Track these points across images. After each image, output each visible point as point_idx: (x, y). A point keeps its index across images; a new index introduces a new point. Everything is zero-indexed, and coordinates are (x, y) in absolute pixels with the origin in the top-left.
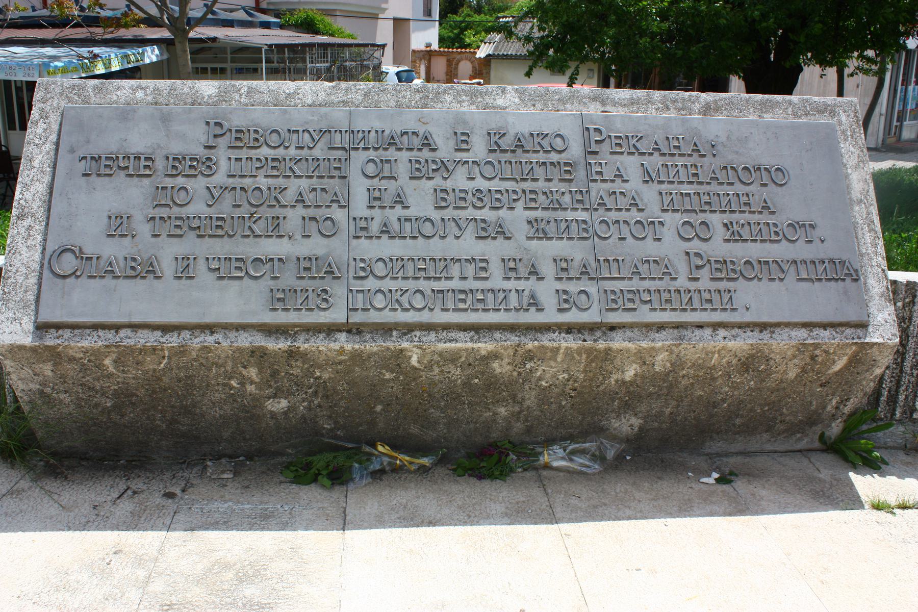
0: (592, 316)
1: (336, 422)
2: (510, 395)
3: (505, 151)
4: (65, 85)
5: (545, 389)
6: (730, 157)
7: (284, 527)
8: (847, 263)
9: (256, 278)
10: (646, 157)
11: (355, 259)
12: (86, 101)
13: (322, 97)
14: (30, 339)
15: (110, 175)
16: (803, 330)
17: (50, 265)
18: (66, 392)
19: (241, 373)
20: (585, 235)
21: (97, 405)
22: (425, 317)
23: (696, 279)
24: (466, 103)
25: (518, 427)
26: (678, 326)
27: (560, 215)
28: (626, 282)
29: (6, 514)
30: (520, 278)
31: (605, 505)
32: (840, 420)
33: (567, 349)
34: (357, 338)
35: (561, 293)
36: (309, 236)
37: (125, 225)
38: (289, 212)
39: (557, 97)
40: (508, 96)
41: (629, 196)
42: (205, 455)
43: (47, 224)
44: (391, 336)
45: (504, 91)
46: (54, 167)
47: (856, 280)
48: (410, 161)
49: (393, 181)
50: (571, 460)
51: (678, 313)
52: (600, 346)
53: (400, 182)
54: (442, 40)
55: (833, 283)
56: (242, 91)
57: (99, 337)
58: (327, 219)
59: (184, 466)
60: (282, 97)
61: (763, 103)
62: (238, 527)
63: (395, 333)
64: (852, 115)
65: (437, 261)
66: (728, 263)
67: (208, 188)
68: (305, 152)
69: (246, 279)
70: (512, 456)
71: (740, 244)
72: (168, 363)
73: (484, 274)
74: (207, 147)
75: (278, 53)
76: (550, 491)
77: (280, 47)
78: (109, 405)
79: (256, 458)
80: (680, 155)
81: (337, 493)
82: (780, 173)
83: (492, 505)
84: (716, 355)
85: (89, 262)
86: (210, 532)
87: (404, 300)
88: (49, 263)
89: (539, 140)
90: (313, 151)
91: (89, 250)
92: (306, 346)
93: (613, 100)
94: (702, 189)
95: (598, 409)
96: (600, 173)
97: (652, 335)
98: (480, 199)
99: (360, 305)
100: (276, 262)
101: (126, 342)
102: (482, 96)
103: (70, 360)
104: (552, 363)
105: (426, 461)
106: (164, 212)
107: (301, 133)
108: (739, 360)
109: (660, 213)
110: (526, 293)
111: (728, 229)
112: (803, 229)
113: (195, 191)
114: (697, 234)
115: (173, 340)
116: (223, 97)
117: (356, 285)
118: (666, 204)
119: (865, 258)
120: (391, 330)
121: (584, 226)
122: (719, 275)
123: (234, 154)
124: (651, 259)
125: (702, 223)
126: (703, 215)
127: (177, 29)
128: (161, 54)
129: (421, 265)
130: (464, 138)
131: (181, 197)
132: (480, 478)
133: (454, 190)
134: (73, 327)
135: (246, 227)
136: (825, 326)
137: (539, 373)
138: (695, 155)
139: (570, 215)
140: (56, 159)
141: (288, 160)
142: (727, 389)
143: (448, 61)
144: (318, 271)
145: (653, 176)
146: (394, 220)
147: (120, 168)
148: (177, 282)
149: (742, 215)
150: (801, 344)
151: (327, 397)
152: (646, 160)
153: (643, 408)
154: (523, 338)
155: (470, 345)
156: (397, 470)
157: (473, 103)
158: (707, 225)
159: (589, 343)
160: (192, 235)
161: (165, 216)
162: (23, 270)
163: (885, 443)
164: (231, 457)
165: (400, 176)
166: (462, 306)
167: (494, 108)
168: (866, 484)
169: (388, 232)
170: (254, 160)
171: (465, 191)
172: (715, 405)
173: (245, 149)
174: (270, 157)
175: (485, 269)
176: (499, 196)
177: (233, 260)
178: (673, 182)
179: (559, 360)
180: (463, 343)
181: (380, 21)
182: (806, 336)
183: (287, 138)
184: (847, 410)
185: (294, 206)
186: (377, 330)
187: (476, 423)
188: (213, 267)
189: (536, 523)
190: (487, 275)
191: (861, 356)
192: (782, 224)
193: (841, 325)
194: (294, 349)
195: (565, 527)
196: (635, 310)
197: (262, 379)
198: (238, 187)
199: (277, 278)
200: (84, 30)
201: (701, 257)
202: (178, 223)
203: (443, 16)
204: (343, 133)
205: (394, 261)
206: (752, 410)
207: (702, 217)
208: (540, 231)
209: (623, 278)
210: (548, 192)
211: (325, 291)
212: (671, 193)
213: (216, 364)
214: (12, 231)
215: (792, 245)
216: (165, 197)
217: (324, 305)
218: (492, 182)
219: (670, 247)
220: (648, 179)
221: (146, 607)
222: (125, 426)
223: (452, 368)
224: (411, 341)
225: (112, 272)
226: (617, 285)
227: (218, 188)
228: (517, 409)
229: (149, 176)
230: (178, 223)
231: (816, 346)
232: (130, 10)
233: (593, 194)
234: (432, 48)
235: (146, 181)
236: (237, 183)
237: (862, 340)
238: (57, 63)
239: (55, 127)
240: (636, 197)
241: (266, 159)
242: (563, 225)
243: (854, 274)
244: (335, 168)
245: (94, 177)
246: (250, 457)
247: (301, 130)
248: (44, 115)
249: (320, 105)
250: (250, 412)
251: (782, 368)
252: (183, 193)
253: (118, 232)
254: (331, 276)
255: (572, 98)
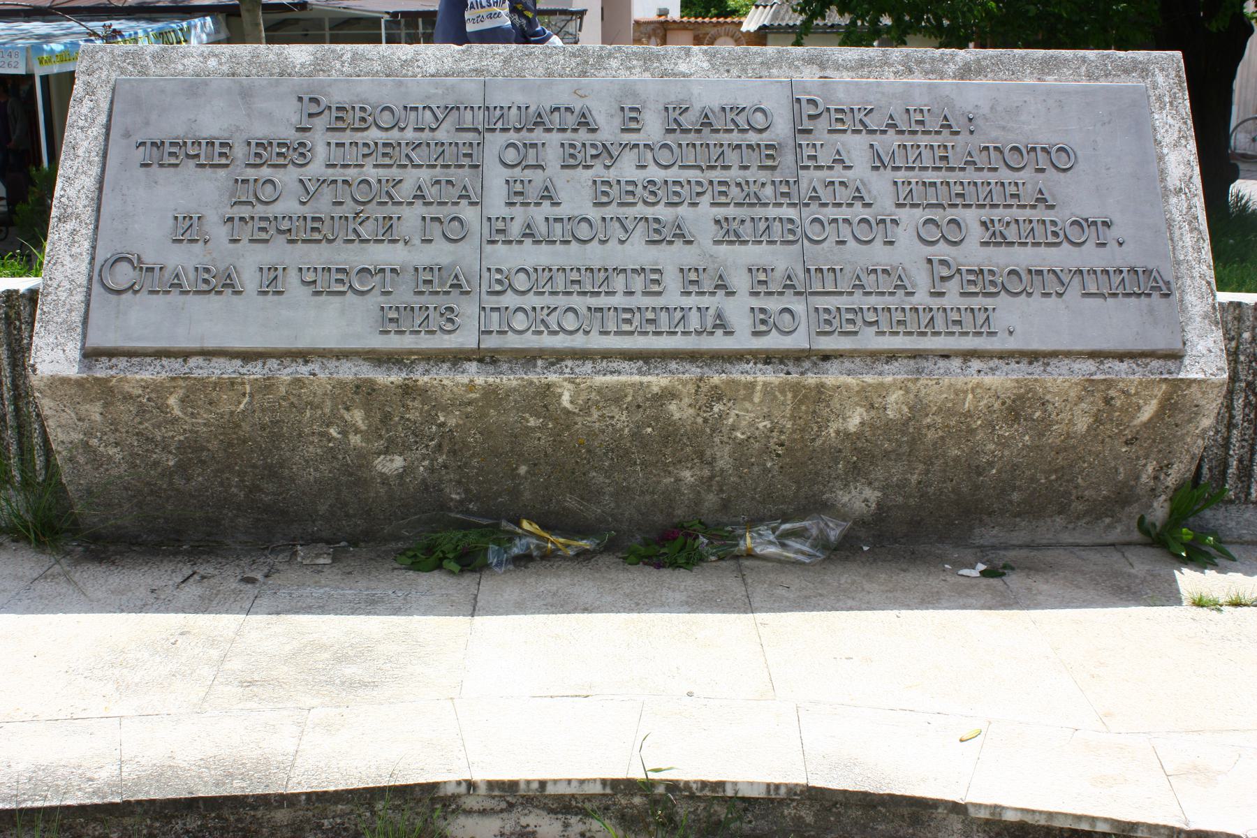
0: (798, 341)
1: (467, 491)
2: (695, 452)
3: (687, 131)
4: (116, 52)
6: (994, 134)
7: (396, 611)
8: (1154, 273)
9: (362, 293)
10: (878, 136)
11: (489, 269)
12: (143, 71)
13: (448, 64)
14: (76, 369)
15: (176, 165)
16: (1091, 361)
18: (117, 444)
19: (342, 417)
20: (791, 238)
21: (156, 464)
22: (579, 342)
23: (941, 294)
24: (638, 70)
26: (916, 355)
27: (759, 212)
29: (41, 597)
30: (703, 293)
31: (821, 595)
32: (1163, 497)
33: (765, 384)
34: (491, 369)
35: (757, 311)
36: (430, 241)
38: (405, 211)
39: (759, 60)
40: (693, 59)
41: (852, 187)
42: (294, 539)
43: (97, 227)
44: (535, 366)
46: (105, 156)
47: (1167, 295)
48: (562, 144)
49: (540, 171)
50: (783, 545)
52: (810, 381)
53: (548, 172)
55: (1133, 299)
56: (344, 58)
57: (163, 367)
58: (453, 219)
59: (266, 552)
60: (397, 65)
61: (1045, 62)
62: (336, 612)
63: (539, 362)
64: (1173, 74)
65: (596, 271)
66: (986, 273)
67: (301, 181)
68: (426, 135)
69: (350, 294)
71: (1003, 248)
72: (250, 403)
73: (656, 288)
74: (298, 130)
75: (408, 26)
76: (750, 581)
78: (171, 463)
79: (362, 544)
80: (924, 132)
81: (468, 580)
82: (1064, 155)
83: (670, 593)
84: (970, 396)
85: (150, 274)
86: (301, 616)
87: (552, 321)
88: (100, 275)
89: (733, 116)
90: (436, 133)
91: (150, 259)
92: (426, 378)
93: (836, 63)
94: (952, 177)
95: (817, 474)
96: (814, 158)
97: (879, 367)
98: (653, 193)
99: (495, 327)
100: (388, 273)
101: (197, 373)
102: (659, 60)
103: (125, 398)
104: (748, 405)
105: (585, 544)
106: (245, 211)
107: (420, 110)
108: (1004, 403)
109: (894, 209)
111: (988, 229)
112: (1093, 228)
114: (943, 236)
115: (256, 371)
116: (319, 65)
117: (492, 301)
118: (902, 196)
119: (1183, 267)
120: (534, 358)
121: (790, 226)
122: (973, 289)
123: (334, 138)
124: (879, 268)
126: (953, 210)
129: (575, 276)
130: (633, 115)
131: (267, 193)
132: (659, 566)
133: (619, 181)
134: (130, 354)
135: (350, 230)
136: (1121, 356)
137: (731, 420)
138: (946, 132)
139: (772, 212)
140: (106, 145)
141: (403, 145)
142: (992, 447)
144: (442, 284)
145: (886, 160)
147: (188, 156)
148: (261, 298)
149: (1008, 211)
150: (1087, 380)
151: (455, 453)
152: (877, 140)
153: (879, 473)
154: (706, 369)
155: (636, 378)
156: (548, 557)
157: (646, 70)
158: (958, 224)
159: (794, 377)
160: (282, 239)
161: (246, 215)
162: (66, 284)
163: (1240, 537)
164: (328, 542)
165: (549, 164)
166: (626, 328)
167: (675, 75)
168: (1189, 580)
169: (532, 235)
170: (360, 145)
171: (634, 183)
172: (979, 471)
173: (348, 131)
174: (380, 142)
175: (657, 282)
176: (678, 189)
177: (333, 271)
178: (913, 168)
179: (756, 400)
180: (628, 376)
182: (1093, 369)
183: (403, 117)
184: (1171, 481)
185: (411, 204)
186: (516, 359)
187: (653, 493)
188: (308, 279)
189: (724, 612)
190: (660, 289)
191: (1176, 400)
192: (1064, 222)
194: (410, 383)
195: (760, 617)
196: (856, 333)
197: (369, 426)
199: (389, 293)
201: (949, 266)
202: (263, 224)
204: (476, 110)
205: (540, 272)
206: (1033, 479)
208: (732, 233)
209: (841, 293)
210: (743, 183)
211: (451, 309)
212: (909, 183)
213: (311, 403)
215: (1077, 249)
216: (246, 193)
217: (449, 327)
219: (907, 252)
220: (879, 163)
221: (221, 683)
222: (192, 496)
223: (615, 411)
224: (561, 373)
225: (180, 285)
227: (314, 181)
228: (706, 473)
229: (226, 166)
230: (263, 224)
231: (1109, 384)
233: (804, 185)
234: (669, 18)
235: (222, 173)
237: (1174, 376)
238: (54, 46)
239: (105, 106)
240: (861, 187)
241: (376, 144)
243: (1164, 287)
244: (465, 155)
245: (155, 167)
246: (354, 542)
247: (421, 106)
249: (446, 75)
250: (354, 474)
251: (1065, 416)
252: (269, 187)
253: (187, 236)
254: (458, 291)
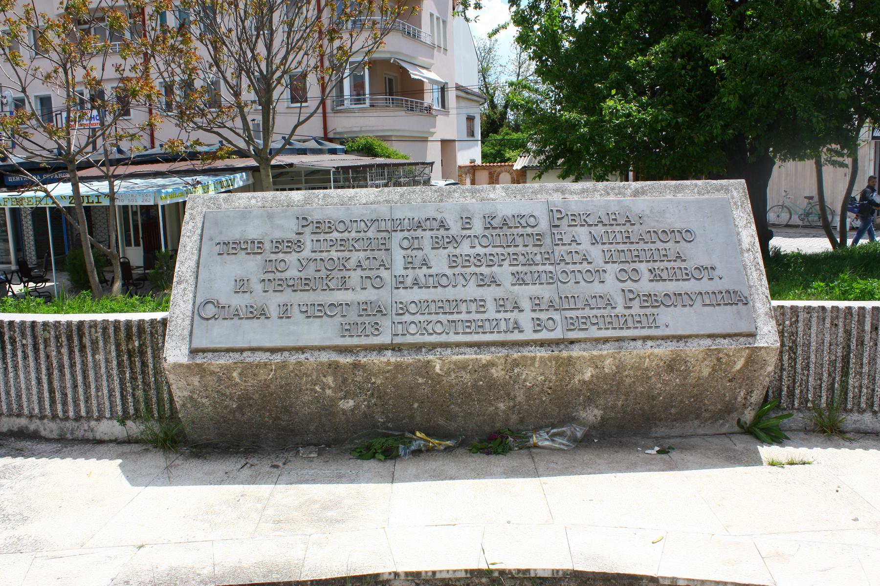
0: (557, 334)
1: (387, 417)
3: (496, 228)
5: (529, 388)
6: (653, 224)
9: (331, 316)
10: (593, 227)
13: (372, 198)
17: (198, 313)
18: (207, 397)
20: (551, 281)
21: (226, 407)
22: (443, 338)
23: (630, 308)
25: (514, 418)
26: (618, 339)
27: (534, 268)
28: (580, 311)
33: (541, 357)
37: (246, 285)
38: (352, 274)
41: (581, 254)
45: (494, 189)
47: (746, 304)
50: (553, 441)
51: (618, 330)
54: (484, 156)
55: (729, 306)
60: (346, 199)
61: (676, 187)
63: (423, 350)
68: (362, 235)
70: (511, 439)
73: (482, 309)
74: (297, 234)
75: (344, 173)
77: (345, 169)
81: (389, 464)
91: (223, 302)
92: (365, 360)
95: (569, 403)
97: (600, 346)
98: (479, 260)
99: (400, 332)
104: (532, 368)
106: (271, 276)
110: (512, 320)
113: (290, 262)
115: (278, 358)
116: (307, 201)
117: (397, 319)
120: (421, 348)
125: (634, 269)
127: (261, 158)
128: (248, 179)
129: (440, 304)
130: (468, 221)
132: (488, 454)
134: (214, 351)
136: (724, 336)
138: (628, 224)
139: (541, 268)
140: (201, 245)
143: (490, 173)
144: (372, 310)
146: (421, 276)
152: (593, 230)
153: (601, 401)
156: (430, 450)
159: (556, 353)
162: (181, 316)
163: (790, 427)
164: (315, 445)
166: (468, 330)
168: (767, 452)
169: (418, 284)
172: (654, 398)
175: (483, 306)
176: (492, 258)
179: (537, 366)
180: (470, 355)
181: (429, 143)
182: (710, 343)
191: (754, 358)
193: (736, 335)
198: (318, 258)
200: (188, 163)
202: (280, 282)
203: (485, 135)
206: (681, 401)
207: (633, 266)
209: (578, 309)
211: (377, 324)
213: (306, 374)
214: (174, 291)
216: (271, 267)
217: (376, 333)
218: (487, 249)
219: (611, 286)
220: (594, 242)
222: (245, 423)
223: (463, 373)
226: (573, 314)
228: (511, 404)
229: (261, 253)
230: (280, 282)
231: (719, 351)
232: (223, 145)
233: (557, 254)
235: (259, 257)
236: (318, 256)
239: (200, 225)
242: (536, 275)
248: (193, 218)
250: (328, 410)
253: (242, 290)
255: (541, 191)
